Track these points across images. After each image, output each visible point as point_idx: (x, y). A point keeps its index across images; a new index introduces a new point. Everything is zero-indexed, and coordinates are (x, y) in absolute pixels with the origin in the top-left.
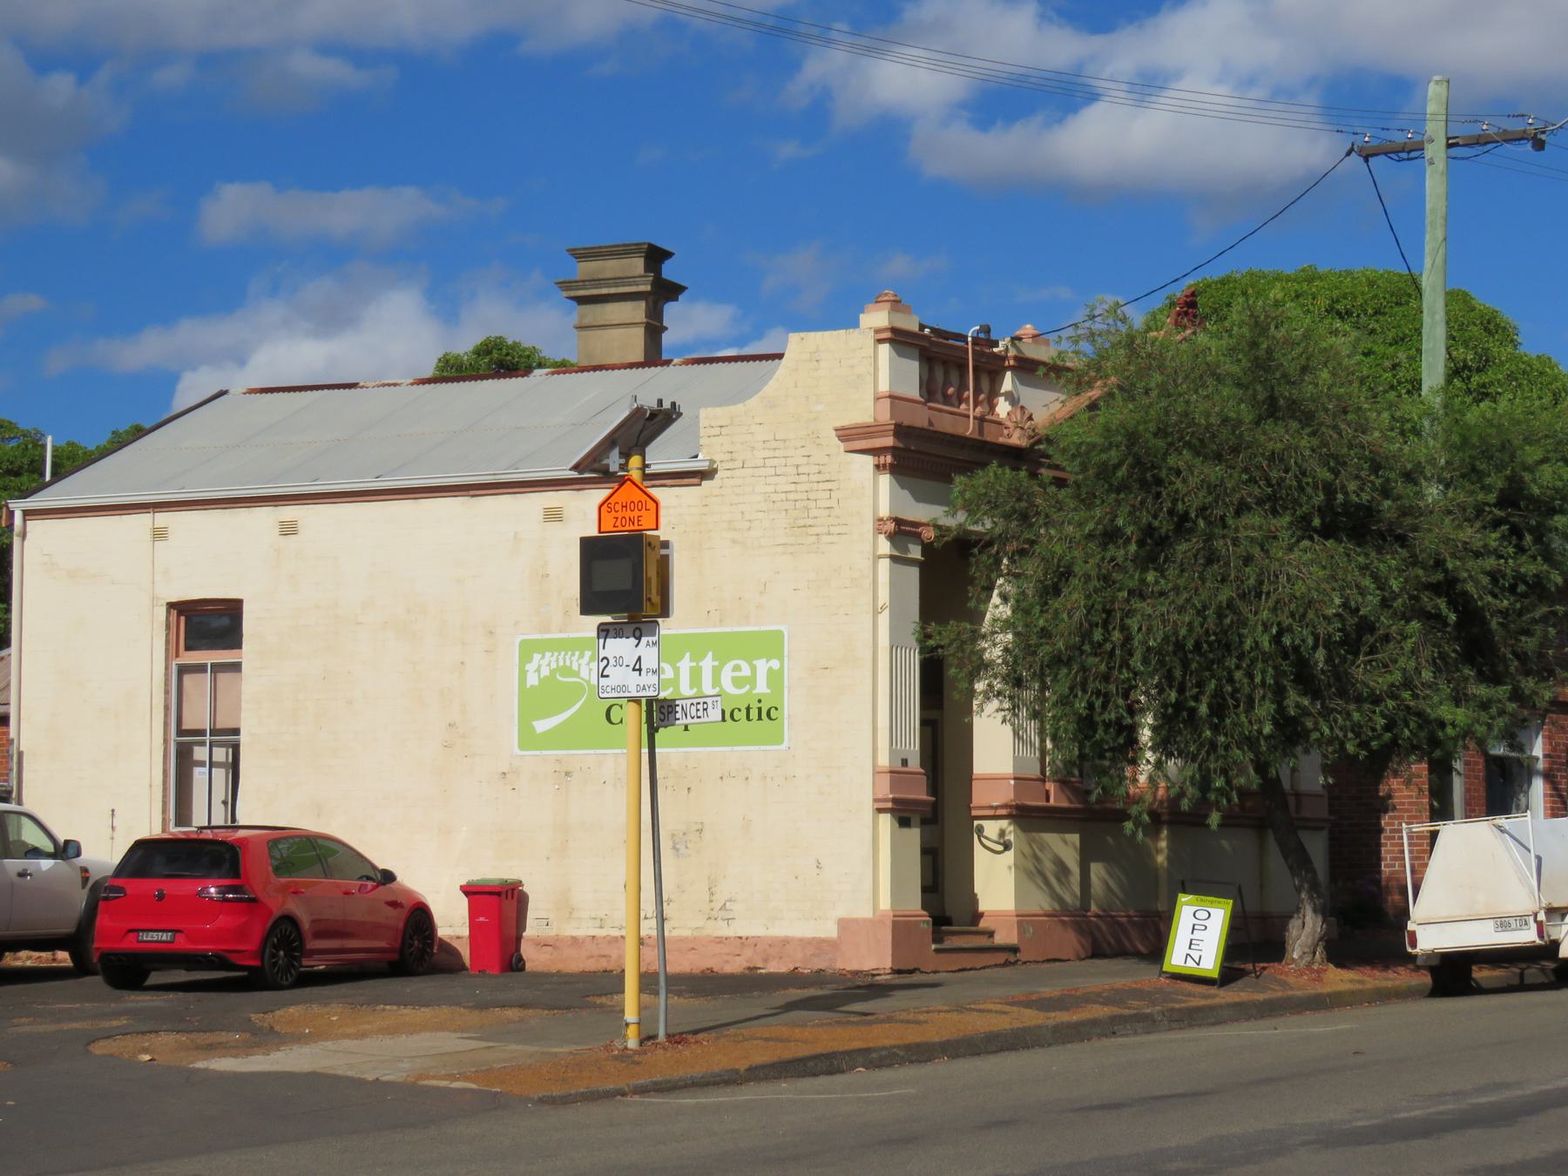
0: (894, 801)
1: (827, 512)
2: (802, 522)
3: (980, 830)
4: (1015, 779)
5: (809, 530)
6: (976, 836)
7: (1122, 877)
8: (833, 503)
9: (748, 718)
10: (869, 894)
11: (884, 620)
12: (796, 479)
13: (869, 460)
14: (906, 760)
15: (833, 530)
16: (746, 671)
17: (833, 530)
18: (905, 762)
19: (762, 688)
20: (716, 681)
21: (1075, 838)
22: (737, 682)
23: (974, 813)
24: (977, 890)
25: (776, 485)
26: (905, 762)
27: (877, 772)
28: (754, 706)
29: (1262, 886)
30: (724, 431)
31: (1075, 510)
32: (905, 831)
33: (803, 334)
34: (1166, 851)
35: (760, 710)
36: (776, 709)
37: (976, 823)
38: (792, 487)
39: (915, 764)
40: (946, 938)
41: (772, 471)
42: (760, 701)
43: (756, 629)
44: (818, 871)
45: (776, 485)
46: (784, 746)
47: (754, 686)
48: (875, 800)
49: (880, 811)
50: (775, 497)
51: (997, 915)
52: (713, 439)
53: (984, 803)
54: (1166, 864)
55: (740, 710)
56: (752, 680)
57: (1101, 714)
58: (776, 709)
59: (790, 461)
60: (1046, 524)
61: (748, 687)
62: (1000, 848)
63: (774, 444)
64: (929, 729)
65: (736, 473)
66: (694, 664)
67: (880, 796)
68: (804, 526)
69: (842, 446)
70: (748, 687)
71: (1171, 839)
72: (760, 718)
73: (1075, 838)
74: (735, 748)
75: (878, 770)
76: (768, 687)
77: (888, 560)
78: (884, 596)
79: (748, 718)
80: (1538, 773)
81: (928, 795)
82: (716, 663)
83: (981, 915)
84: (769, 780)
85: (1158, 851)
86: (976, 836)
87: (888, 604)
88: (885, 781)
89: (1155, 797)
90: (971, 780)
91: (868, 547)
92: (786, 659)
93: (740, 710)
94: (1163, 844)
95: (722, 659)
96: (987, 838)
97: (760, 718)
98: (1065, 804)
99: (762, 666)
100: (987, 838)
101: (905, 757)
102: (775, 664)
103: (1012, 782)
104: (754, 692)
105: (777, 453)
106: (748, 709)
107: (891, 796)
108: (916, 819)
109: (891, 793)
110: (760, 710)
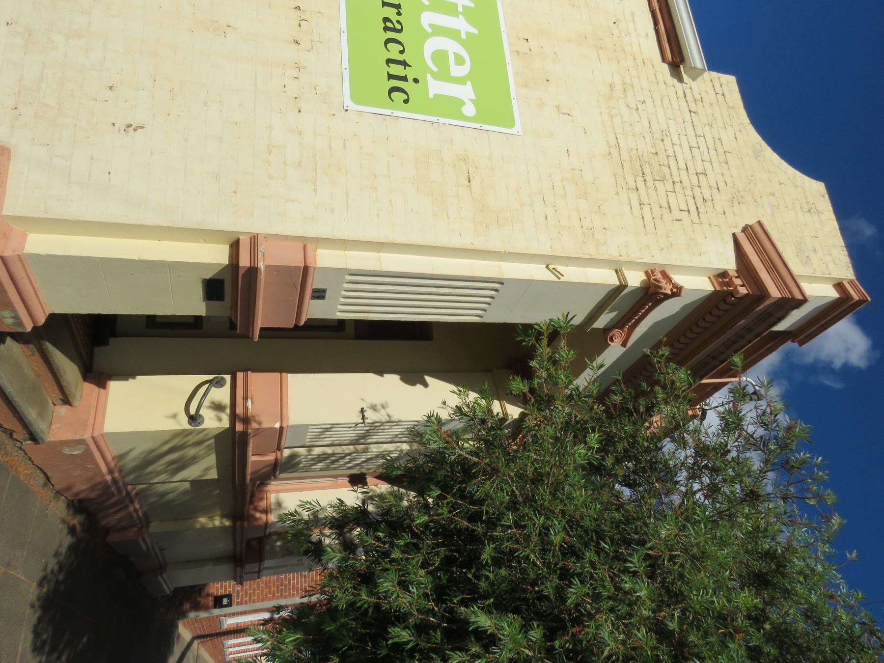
0: (253, 271)
1: (665, 205)
2: (647, 171)
3: (219, 383)
4: (281, 428)
5: (640, 179)
6: (210, 377)
7: (178, 502)
8: (676, 214)
9: (389, 61)
10: (57, 211)
11: (538, 272)
12: (692, 171)
13: (729, 263)
14: (323, 297)
15: (646, 209)
16: (457, 71)
17: (646, 209)
18: (319, 294)
19: (435, 87)
20: (439, 31)
21: (213, 475)
22: (440, 56)
23: (240, 376)
24: (140, 378)
25: (680, 146)
26: (319, 294)
27: (306, 243)
28: (410, 73)
29: (188, 562)
30: (720, 97)
31: (699, 559)
32: (199, 291)
33: (827, 196)
34: (211, 526)
35: (404, 79)
36: (406, 101)
37: (228, 378)
38: (682, 165)
39: (315, 310)
40: (31, 346)
41: (694, 144)
42: (416, 81)
43: (513, 95)
44: (121, 123)
45: (680, 146)
46: (348, 102)
47: (436, 77)
48: (254, 240)
49: (235, 246)
50: (667, 141)
51: (100, 409)
52: (710, 84)
53: (252, 389)
54: (198, 526)
55: (402, 52)
56: (444, 75)
57: (410, 641)
58: (406, 101)
59: (707, 165)
60: (501, 430)
61: (435, 69)
62: (193, 411)
63: (721, 151)
64: (336, 324)
65: (683, 103)
66: (460, 9)
67: (261, 248)
68: (644, 173)
69: (738, 231)
70: (435, 69)
71: (223, 528)
72: (391, 77)
73: (213, 475)
74: (344, 37)
75: (310, 247)
76: (436, 95)
77: (614, 281)
78: (572, 274)
79: (389, 61)
80: (272, 615)
81: (252, 473)
82: (464, 36)
83: (102, 384)
84: (295, 73)
85: (211, 519)
86: (210, 377)
87: (562, 279)
88: (293, 258)
89: (265, 534)
90: (281, 372)
91: (635, 255)
92: (478, 126)
93: (402, 52)
94: (217, 523)
95: (468, 43)
96: (207, 390)
97: (391, 77)
98: (249, 470)
99: (466, 92)
100: (207, 390)
101: (328, 295)
102: (469, 110)
103: (277, 425)
104: (429, 76)
105: (712, 152)
106: (404, 63)
107: (261, 265)
108: (221, 309)
109: (267, 267)
110: (404, 79)
